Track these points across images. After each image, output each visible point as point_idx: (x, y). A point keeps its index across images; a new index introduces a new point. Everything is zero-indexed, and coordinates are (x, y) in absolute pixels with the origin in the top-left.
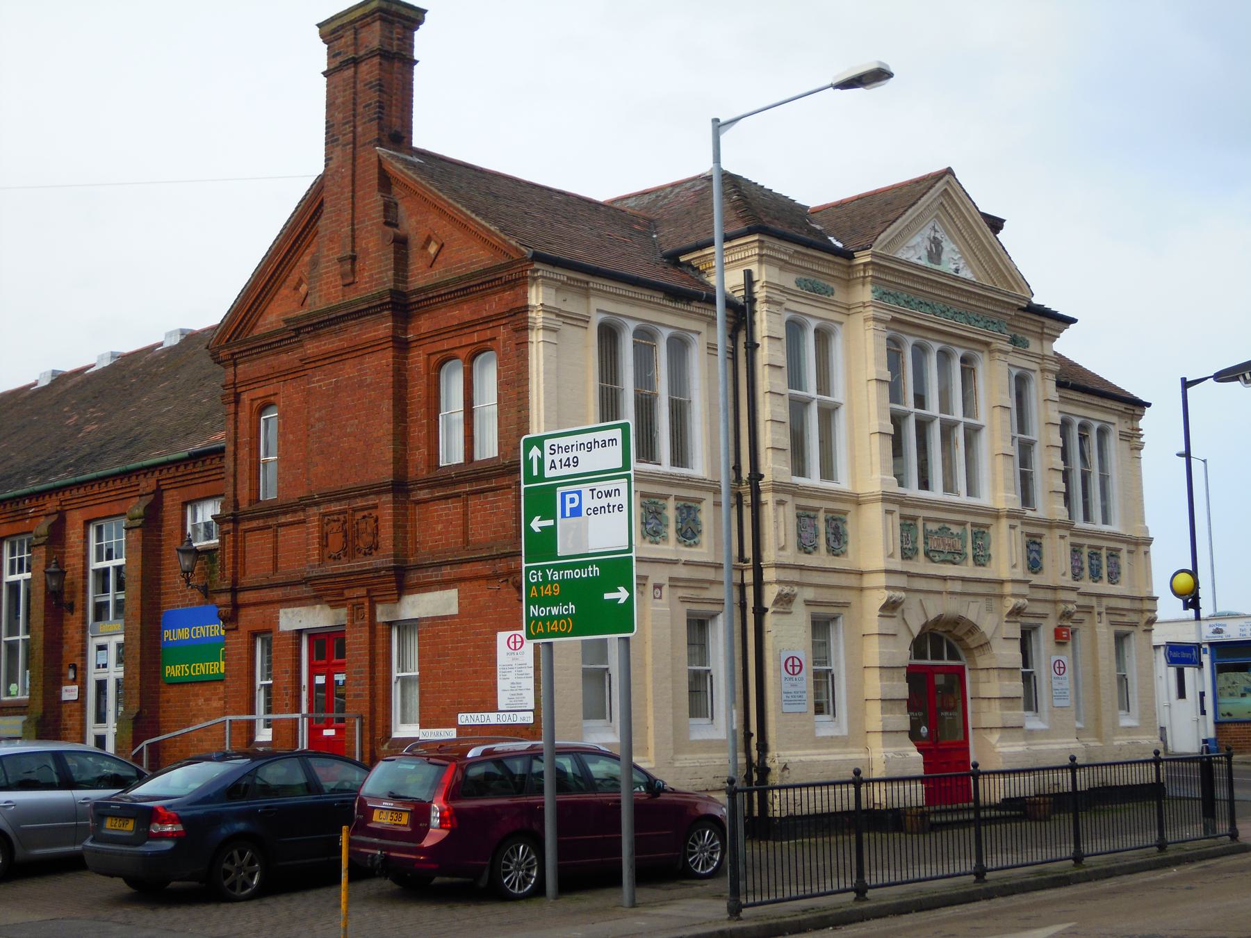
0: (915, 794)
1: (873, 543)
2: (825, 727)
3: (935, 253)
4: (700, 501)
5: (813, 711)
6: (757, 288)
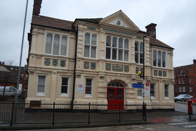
1: (101, 68)
2: (88, 96)
3: (119, 23)
4: (66, 60)
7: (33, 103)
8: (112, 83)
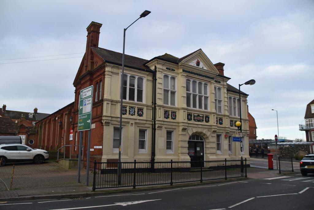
0: (189, 165)
1: (181, 117)
2: (169, 152)
3: (198, 64)
5: (112, 147)
6: (157, 69)
7: (110, 162)
8: (194, 136)
